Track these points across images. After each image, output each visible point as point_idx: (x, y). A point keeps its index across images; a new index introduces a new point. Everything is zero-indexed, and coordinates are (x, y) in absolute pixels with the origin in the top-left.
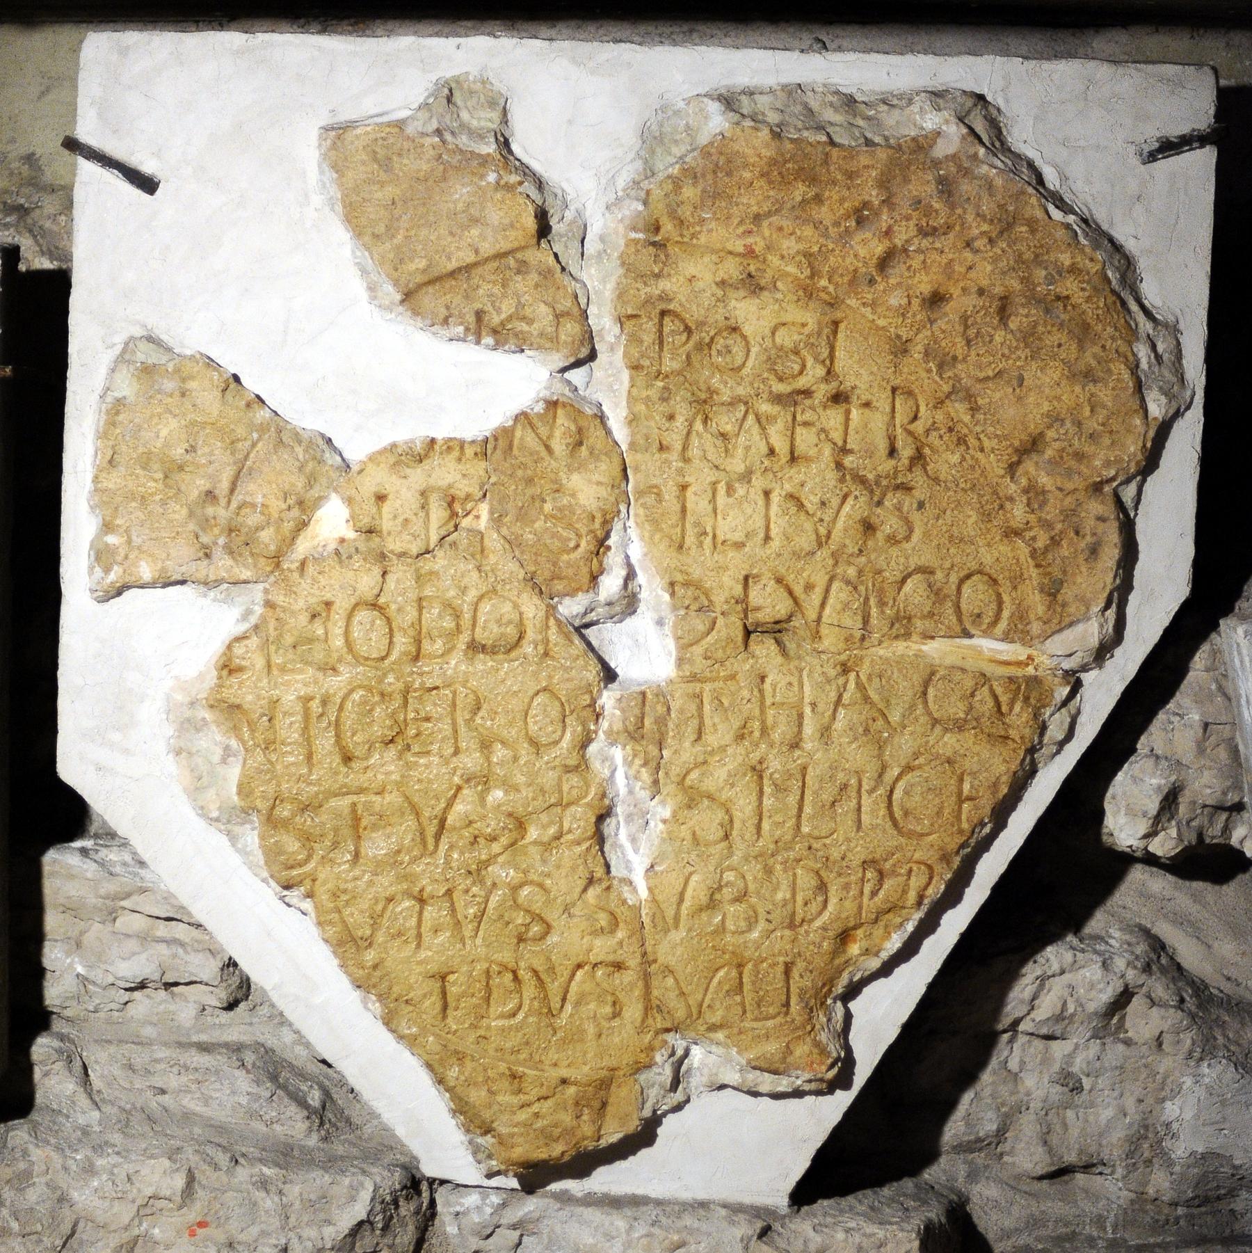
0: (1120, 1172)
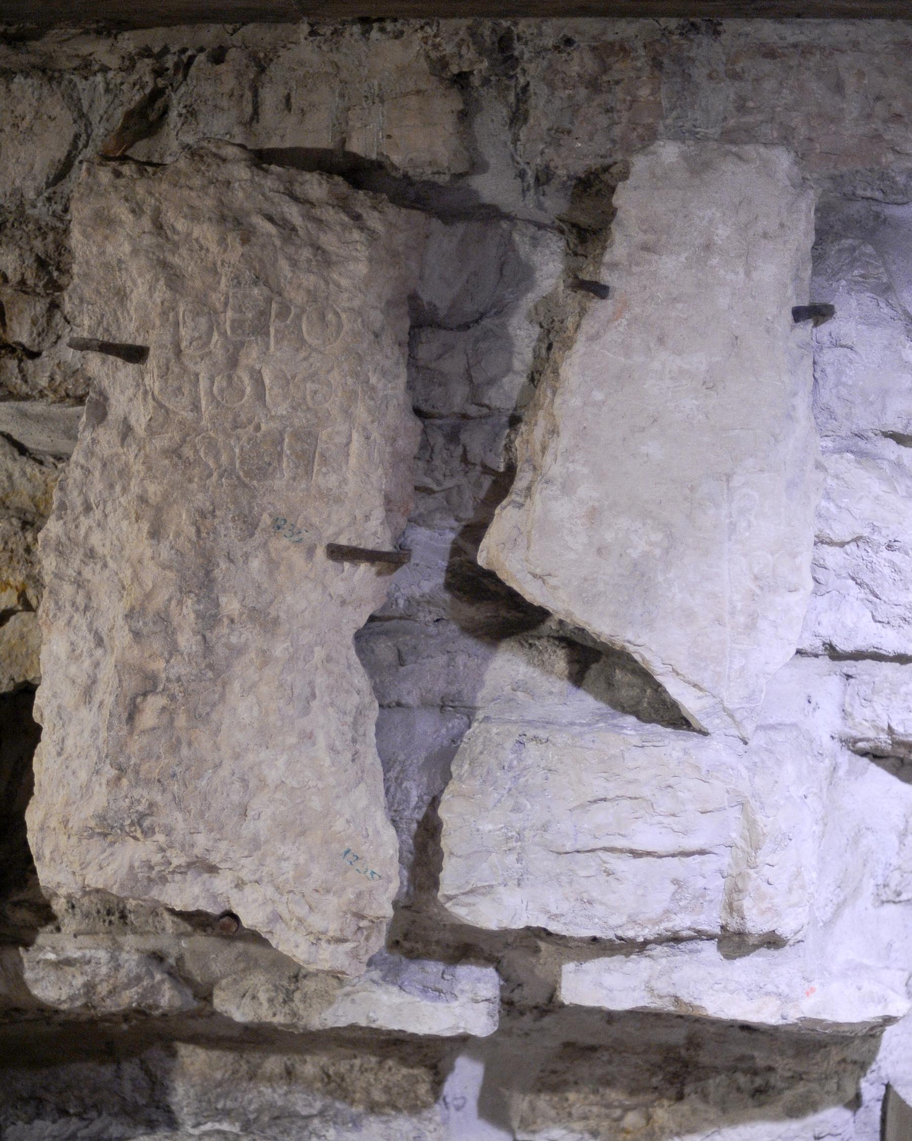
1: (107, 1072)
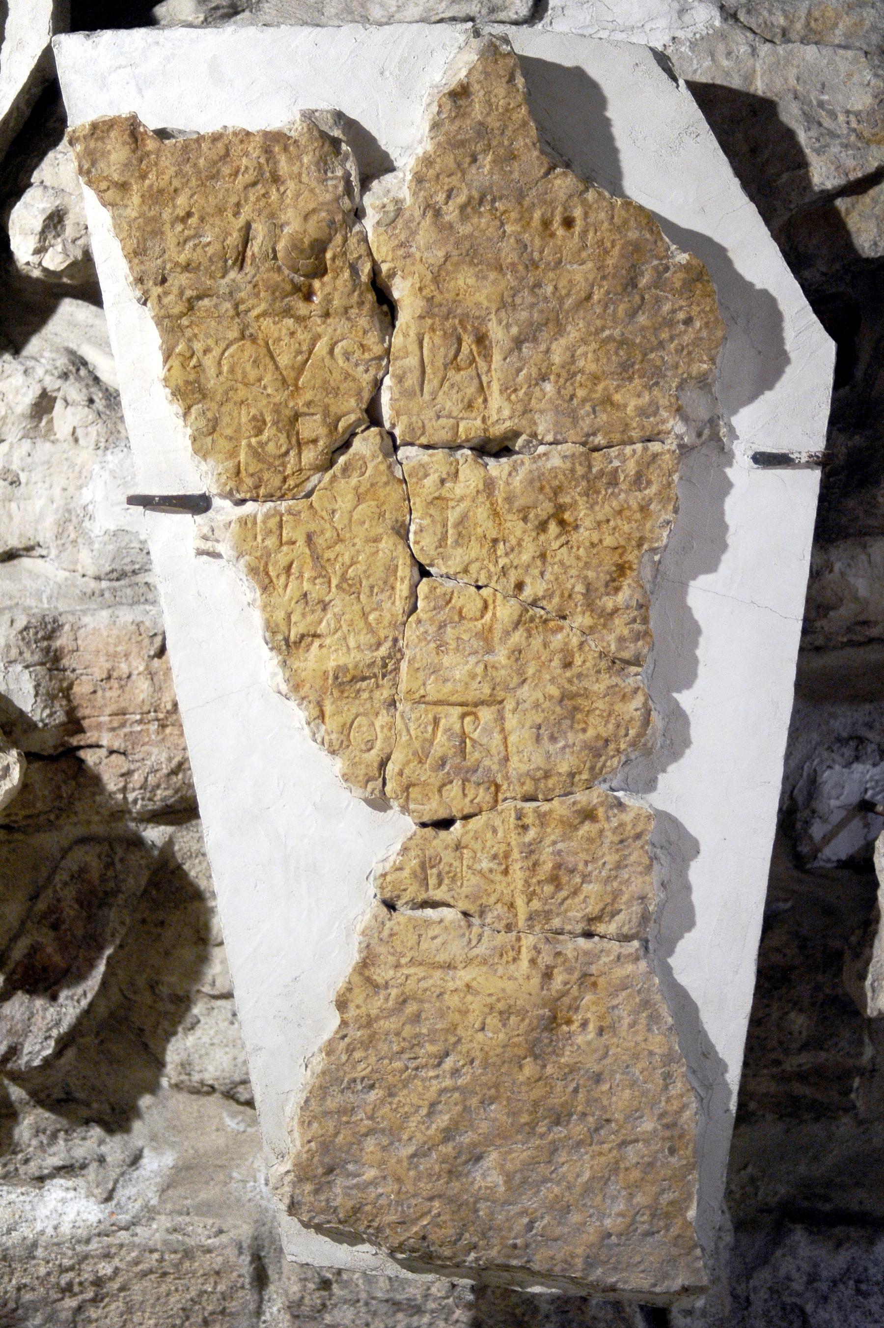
0: (54, 552)
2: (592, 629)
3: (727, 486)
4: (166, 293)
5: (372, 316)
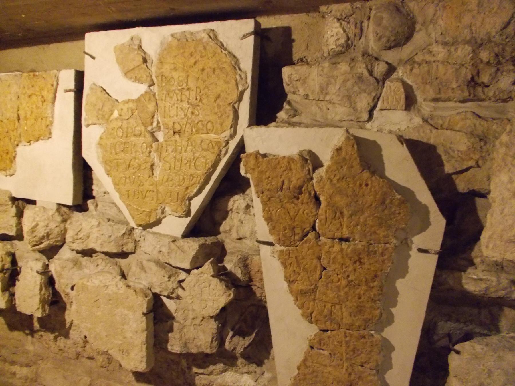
0: (249, 240)
1: (475, 311)
2: (367, 290)
3: (409, 256)
4: (264, 196)
5: (314, 205)
